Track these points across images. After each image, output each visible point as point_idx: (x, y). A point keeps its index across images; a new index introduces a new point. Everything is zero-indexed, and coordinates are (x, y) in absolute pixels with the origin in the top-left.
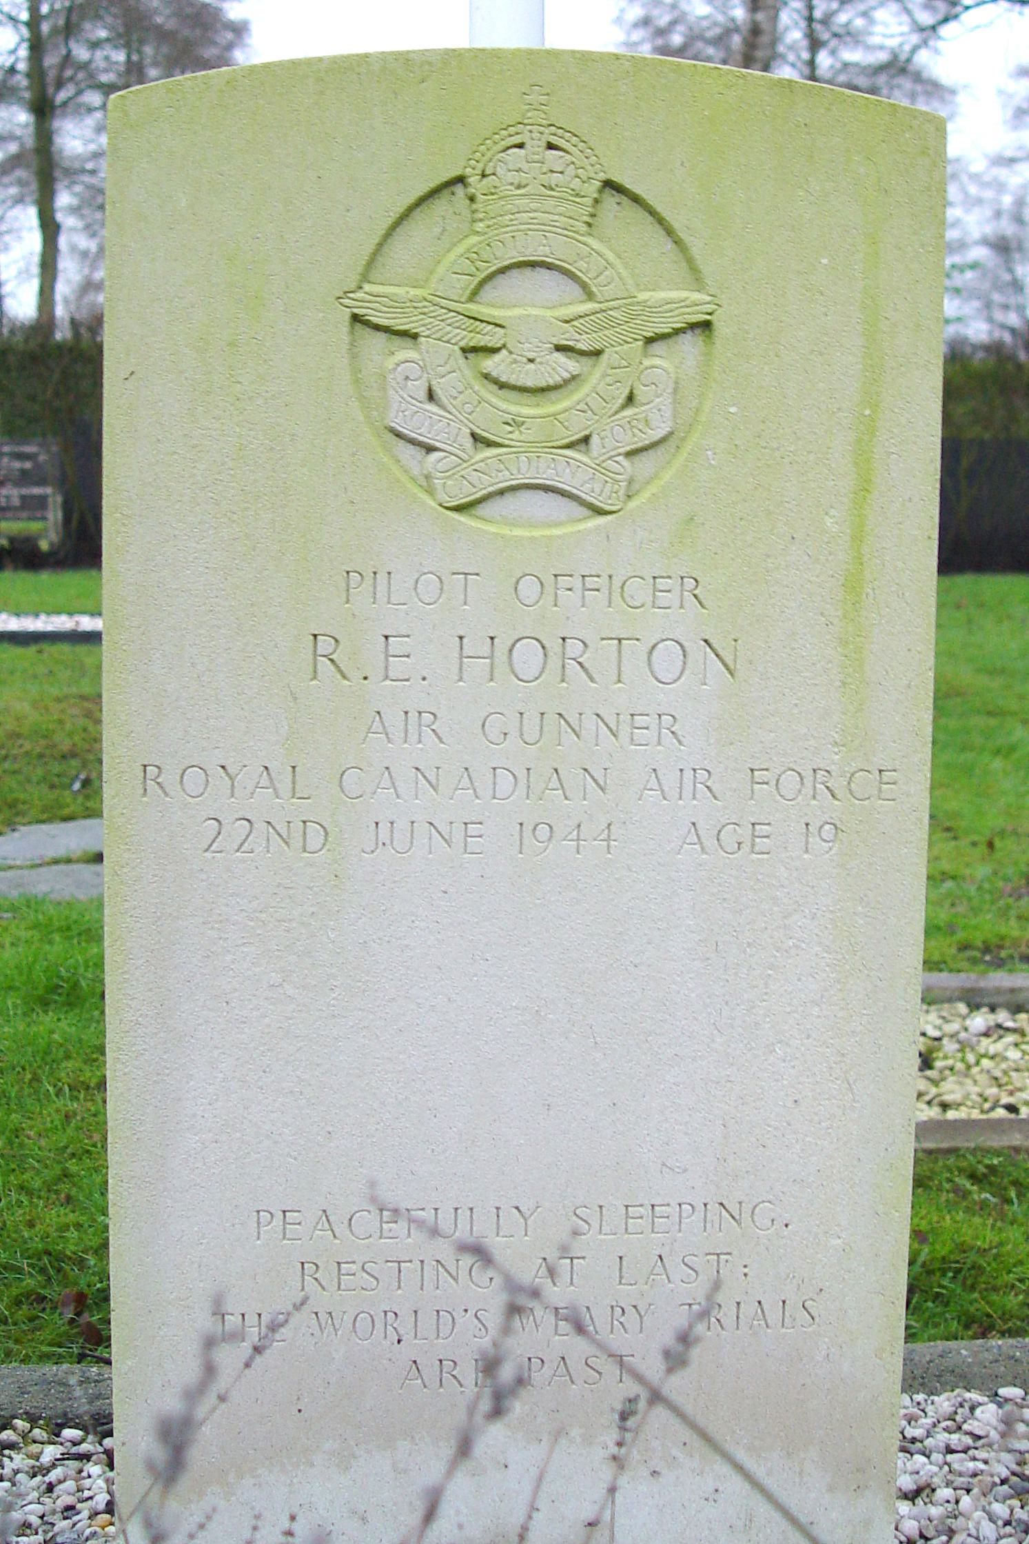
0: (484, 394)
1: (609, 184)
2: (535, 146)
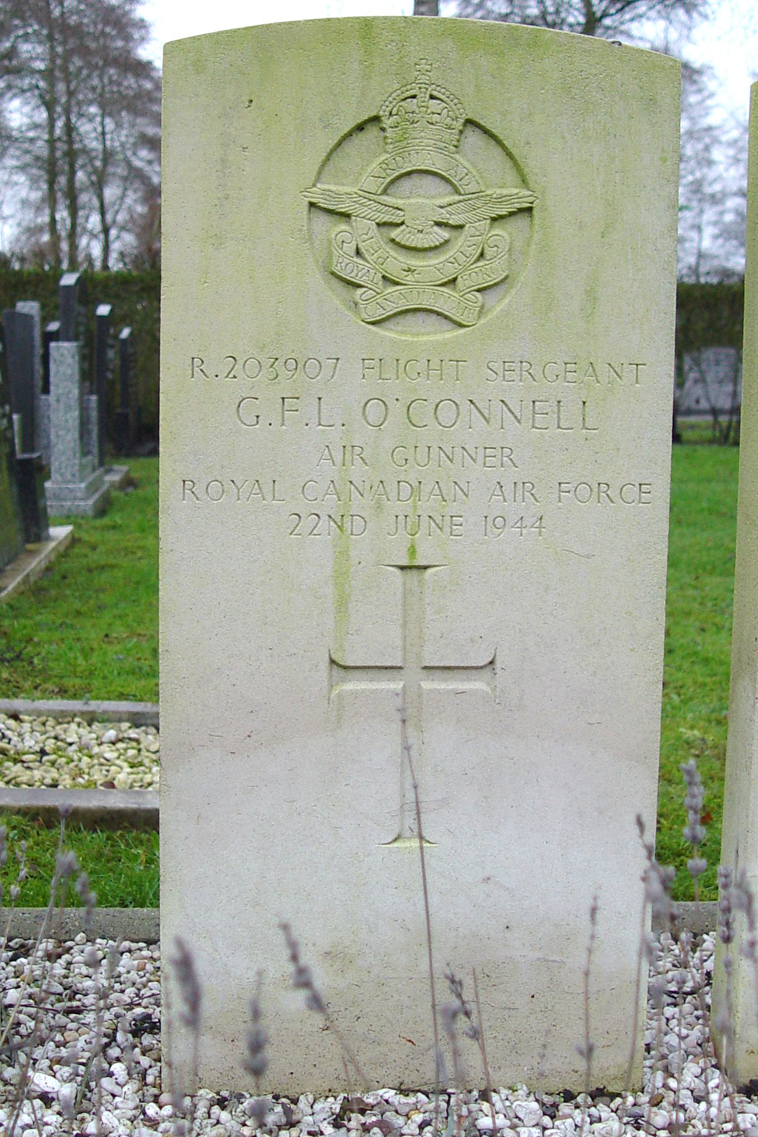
0: (392, 253)
1: (469, 122)
2: (423, 97)
